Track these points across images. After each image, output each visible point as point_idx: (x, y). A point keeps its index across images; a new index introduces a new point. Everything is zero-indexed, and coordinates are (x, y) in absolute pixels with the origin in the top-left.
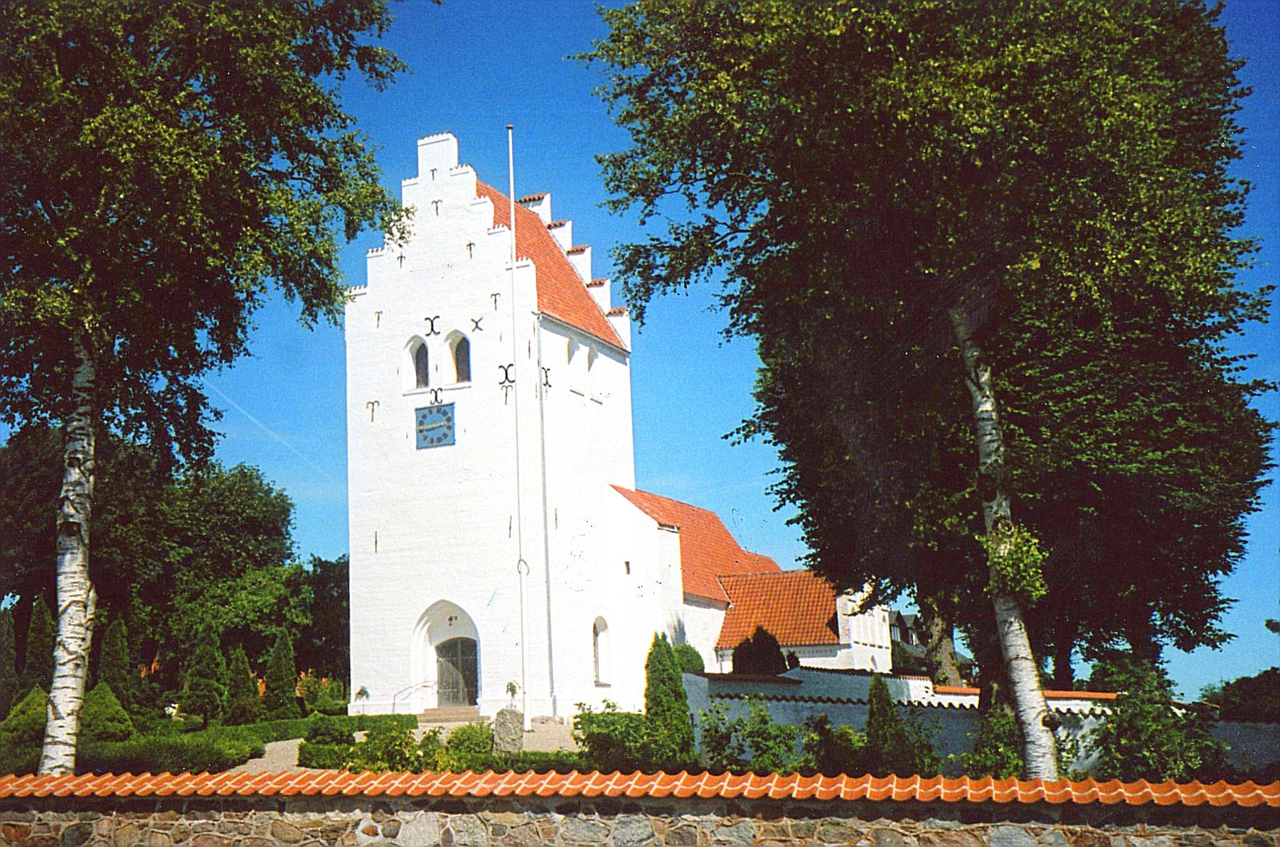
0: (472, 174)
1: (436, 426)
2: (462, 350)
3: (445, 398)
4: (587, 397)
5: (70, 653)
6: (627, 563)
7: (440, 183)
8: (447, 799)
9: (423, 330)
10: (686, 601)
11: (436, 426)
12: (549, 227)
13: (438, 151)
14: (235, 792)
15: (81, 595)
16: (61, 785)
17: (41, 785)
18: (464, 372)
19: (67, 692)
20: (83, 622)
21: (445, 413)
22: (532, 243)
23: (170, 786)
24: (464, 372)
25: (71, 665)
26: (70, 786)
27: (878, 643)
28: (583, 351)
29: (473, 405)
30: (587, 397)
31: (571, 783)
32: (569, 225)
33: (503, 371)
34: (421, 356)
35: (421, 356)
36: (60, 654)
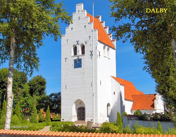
0: (86, 12)
1: (78, 64)
2: (83, 48)
3: (80, 58)
4: (107, 58)
5: (9, 107)
6: (114, 92)
7: (80, 13)
8: (52, 136)
9: (76, 44)
10: (125, 100)
11: (78, 64)
12: (101, 22)
13: (80, 7)
14: (27, 134)
15: (11, 95)
16: (8, 132)
17: (4, 131)
18: (83, 52)
19: (9, 113)
20: (11, 101)
21: (80, 61)
22: (97, 26)
23: (26, 133)
24: (83, 52)
25: (9, 109)
26: (9, 132)
27: (161, 109)
28: (107, 47)
29: (85, 59)
30: (107, 58)
31: (94, 135)
32: (104, 22)
33: (77, 42)
34: (75, 49)
35: (75, 49)
36: (8, 107)
